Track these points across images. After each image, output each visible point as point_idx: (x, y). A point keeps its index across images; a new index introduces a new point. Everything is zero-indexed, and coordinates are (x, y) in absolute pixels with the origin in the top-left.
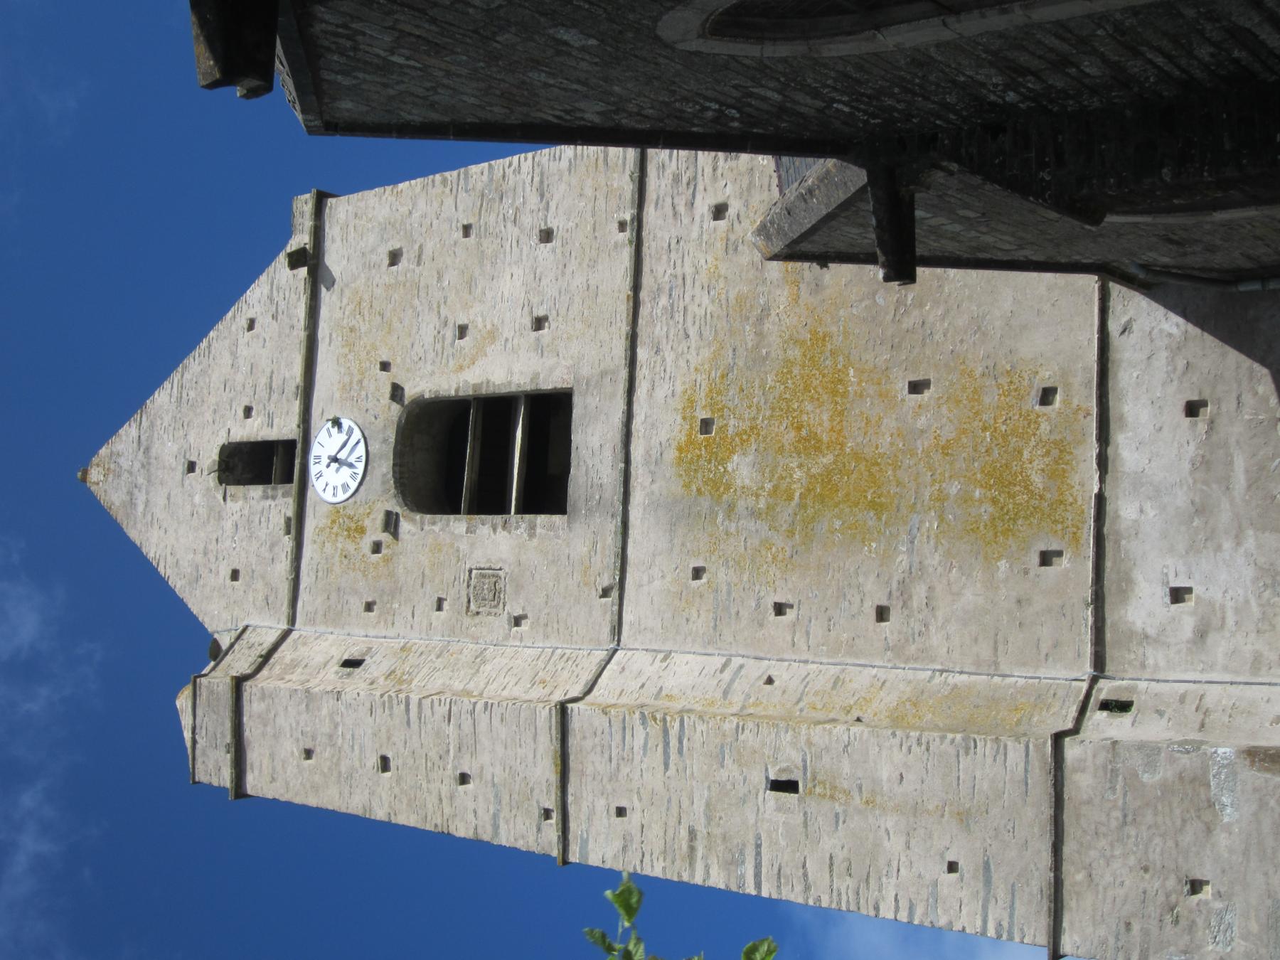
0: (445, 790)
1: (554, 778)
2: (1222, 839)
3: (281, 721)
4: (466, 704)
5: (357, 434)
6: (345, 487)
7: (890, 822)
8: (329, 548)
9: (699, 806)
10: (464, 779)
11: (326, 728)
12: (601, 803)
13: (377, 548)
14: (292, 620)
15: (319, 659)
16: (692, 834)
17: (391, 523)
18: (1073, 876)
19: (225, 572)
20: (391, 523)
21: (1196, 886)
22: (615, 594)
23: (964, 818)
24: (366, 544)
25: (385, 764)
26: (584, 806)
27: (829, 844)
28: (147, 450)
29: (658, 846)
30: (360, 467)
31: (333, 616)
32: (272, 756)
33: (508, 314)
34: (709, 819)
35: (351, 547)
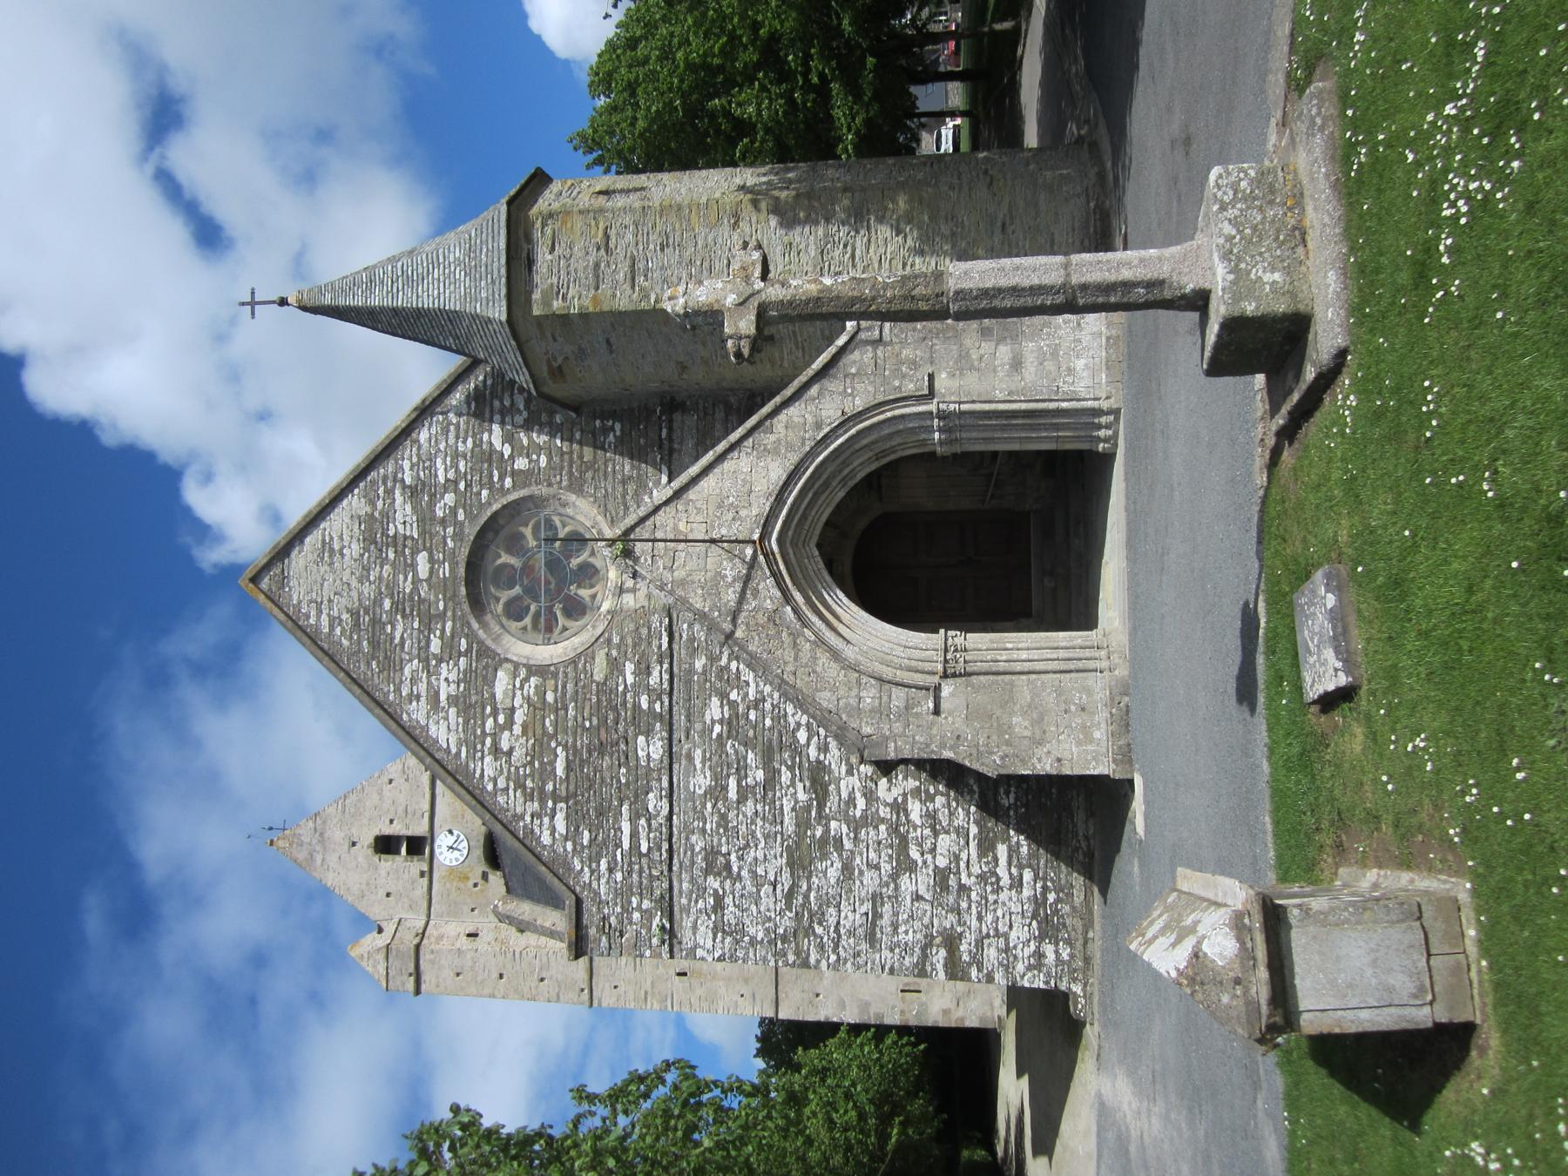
0: (533, 985)
1: (586, 977)
2: (825, 982)
3: (443, 962)
4: (544, 951)
5: (462, 837)
6: (457, 860)
7: (721, 983)
8: (448, 885)
9: (649, 983)
10: (542, 980)
11: (470, 963)
12: (607, 985)
13: (475, 885)
14: (429, 916)
15: (453, 933)
16: (646, 993)
17: (485, 876)
18: (782, 995)
19: (382, 893)
20: (485, 876)
21: (818, 995)
22: (427, 875)
23: (746, 981)
24: (471, 883)
25: (501, 976)
26: (600, 986)
27: (699, 992)
28: (321, 834)
29: (632, 998)
30: (465, 852)
31: (454, 912)
32: (437, 977)
33: (760, 855)
34: (653, 987)
35: (462, 885)
